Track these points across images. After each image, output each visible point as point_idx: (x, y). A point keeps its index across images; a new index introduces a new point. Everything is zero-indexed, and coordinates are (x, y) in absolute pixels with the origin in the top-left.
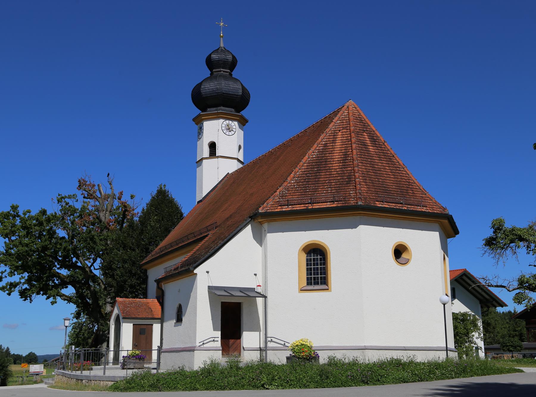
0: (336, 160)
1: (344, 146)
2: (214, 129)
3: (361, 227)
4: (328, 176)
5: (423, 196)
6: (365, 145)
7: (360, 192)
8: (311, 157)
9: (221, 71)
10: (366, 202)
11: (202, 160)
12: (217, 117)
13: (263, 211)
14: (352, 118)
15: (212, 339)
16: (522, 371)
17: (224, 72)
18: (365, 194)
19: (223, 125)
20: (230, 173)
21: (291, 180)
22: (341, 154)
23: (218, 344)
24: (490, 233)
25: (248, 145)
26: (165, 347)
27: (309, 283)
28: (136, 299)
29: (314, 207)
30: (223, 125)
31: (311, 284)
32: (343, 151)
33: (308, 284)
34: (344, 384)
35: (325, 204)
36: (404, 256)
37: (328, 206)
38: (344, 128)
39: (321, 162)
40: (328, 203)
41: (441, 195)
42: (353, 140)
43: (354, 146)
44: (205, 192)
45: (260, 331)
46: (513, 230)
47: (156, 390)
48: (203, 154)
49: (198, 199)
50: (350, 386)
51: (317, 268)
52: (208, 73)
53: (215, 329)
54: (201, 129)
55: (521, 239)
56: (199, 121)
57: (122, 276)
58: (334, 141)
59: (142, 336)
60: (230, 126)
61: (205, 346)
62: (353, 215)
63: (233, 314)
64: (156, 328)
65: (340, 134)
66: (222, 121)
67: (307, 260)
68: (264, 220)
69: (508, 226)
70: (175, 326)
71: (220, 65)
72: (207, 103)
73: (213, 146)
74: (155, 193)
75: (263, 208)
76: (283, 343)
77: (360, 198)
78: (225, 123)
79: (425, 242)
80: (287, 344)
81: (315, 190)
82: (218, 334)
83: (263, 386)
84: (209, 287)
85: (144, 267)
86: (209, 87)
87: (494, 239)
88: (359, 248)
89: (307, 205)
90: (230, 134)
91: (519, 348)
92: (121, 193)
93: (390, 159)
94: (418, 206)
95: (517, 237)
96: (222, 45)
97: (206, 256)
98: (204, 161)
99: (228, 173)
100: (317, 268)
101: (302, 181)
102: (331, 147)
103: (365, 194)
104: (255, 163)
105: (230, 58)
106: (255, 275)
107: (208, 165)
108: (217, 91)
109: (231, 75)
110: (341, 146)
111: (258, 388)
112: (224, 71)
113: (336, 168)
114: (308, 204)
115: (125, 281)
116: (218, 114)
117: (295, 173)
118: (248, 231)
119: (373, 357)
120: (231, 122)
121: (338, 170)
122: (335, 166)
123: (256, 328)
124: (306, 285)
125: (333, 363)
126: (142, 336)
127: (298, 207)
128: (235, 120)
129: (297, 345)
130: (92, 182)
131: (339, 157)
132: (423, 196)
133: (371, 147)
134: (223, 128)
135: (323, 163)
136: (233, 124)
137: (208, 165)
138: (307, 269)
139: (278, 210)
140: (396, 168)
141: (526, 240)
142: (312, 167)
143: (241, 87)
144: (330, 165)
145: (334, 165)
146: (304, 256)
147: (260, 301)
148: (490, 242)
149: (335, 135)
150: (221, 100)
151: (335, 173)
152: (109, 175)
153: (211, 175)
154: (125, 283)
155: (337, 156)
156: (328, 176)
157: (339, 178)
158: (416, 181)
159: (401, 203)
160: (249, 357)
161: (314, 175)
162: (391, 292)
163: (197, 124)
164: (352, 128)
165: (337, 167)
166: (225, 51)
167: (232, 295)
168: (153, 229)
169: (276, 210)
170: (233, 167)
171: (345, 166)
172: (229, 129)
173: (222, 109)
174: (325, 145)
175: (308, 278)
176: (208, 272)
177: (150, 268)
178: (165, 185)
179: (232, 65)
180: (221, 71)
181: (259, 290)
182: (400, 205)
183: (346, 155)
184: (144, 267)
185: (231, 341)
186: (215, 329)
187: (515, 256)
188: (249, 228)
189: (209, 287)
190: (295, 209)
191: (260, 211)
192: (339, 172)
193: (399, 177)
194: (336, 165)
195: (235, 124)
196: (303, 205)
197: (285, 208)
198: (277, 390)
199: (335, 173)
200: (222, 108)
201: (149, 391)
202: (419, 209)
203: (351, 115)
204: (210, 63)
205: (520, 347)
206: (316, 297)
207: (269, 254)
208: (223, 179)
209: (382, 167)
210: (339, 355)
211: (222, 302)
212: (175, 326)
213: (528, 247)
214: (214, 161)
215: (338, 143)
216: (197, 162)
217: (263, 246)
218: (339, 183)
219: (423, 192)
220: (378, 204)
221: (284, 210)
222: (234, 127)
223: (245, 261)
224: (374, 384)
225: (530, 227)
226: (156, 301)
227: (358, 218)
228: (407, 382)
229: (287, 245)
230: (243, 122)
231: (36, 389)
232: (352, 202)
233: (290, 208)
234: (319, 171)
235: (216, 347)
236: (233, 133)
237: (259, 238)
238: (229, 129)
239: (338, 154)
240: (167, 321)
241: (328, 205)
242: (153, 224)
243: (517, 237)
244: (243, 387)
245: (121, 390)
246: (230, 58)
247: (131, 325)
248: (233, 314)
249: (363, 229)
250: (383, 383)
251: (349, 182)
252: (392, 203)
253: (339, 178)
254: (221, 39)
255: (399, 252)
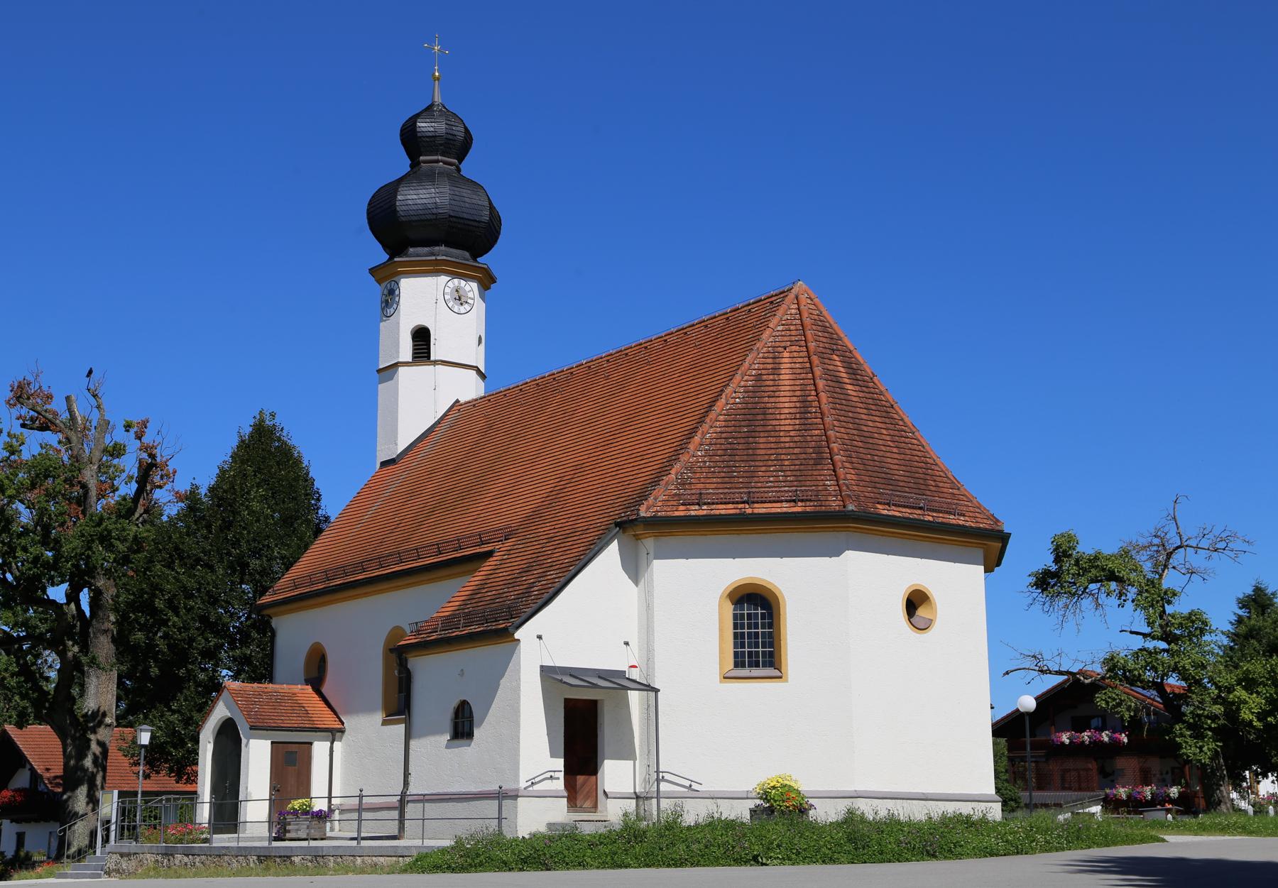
0: (786, 411)
1: (798, 382)
2: (425, 297)
3: (849, 554)
4: (772, 445)
5: (955, 491)
6: (838, 381)
7: (842, 485)
8: (732, 401)
9: (437, 161)
10: (859, 505)
11: (396, 365)
12: (434, 269)
13: (648, 515)
14: (807, 321)
15: (548, 775)
16: (1164, 840)
17: (445, 163)
18: (855, 488)
19: (447, 290)
20: (462, 401)
21: (696, 450)
22: (795, 399)
23: (559, 785)
24: (1047, 561)
25: (493, 338)
26: (413, 790)
27: (739, 663)
28: (266, 685)
29: (756, 511)
30: (447, 290)
31: (743, 666)
32: (798, 393)
33: (736, 665)
34: (898, 858)
35: (779, 505)
36: (921, 612)
37: (785, 510)
38: (793, 343)
39: (754, 415)
40: (785, 504)
41: (988, 491)
42: (818, 371)
43: (821, 384)
44: (404, 440)
45: (634, 759)
46: (1096, 558)
47: (537, 869)
48: (398, 352)
49: (383, 456)
50: (907, 860)
51: (756, 632)
52: (404, 165)
53: (553, 755)
54: (390, 299)
55: (1112, 576)
56: (386, 277)
57: (186, 628)
58: (776, 371)
59: (291, 769)
60: (461, 292)
61: (536, 787)
62: (834, 529)
63: (583, 728)
64: (320, 749)
65: (786, 354)
66: (444, 279)
67: (735, 616)
68: (644, 529)
69: (1085, 548)
70: (447, 747)
71: (432, 145)
72: (403, 237)
73: (422, 337)
74: (247, 430)
75: (648, 508)
76: (687, 783)
77: (849, 496)
78: (450, 284)
79: (958, 584)
80: (695, 786)
81: (752, 475)
82: (559, 763)
83: (755, 858)
84: (542, 667)
85: (266, 612)
86: (414, 198)
87: (1056, 575)
88: (838, 593)
89: (740, 506)
90: (462, 309)
91: (1013, 803)
92: (144, 424)
93: (886, 411)
94: (950, 513)
95: (1105, 573)
96: (438, 99)
97: (540, 602)
98: (402, 371)
99: (457, 401)
100: (756, 632)
101: (719, 452)
102: (771, 383)
103: (855, 488)
104: (546, 387)
105: (459, 132)
106: (627, 644)
107: (411, 379)
108: (435, 211)
109: (459, 170)
110: (792, 382)
111: (746, 862)
112: (440, 162)
113: (787, 428)
114: (743, 502)
115: (191, 640)
116: (437, 262)
117: (704, 434)
118: (611, 555)
119: (917, 812)
120: (463, 283)
121: (792, 433)
122: (786, 424)
123: (627, 753)
124: (732, 666)
125: (851, 821)
126: (291, 769)
127: (722, 510)
128: (472, 278)
129: (774, 787)
130: (45, 388)
131: (792, 405)
132: (955, 491)
133: (849, 387)
134: (447, 297)
135: (759, 417)
136: (467, 288)
137: (411, 379)
138: (736, 635)
139: (682, 514)
140: (900, 433)
141: (1119, 580)
142: (737, 423)
143: (487, 204)
144: (774, 423)
145: (783, 422)
146: (729, 608)
147: (634, 697)
148: (1044, 581)
149: (776, 358)
150: (432, 228)
151: (788, 439)
152: (90, 372)
153: (419, 403)
154: (190, 646)
155: (786, 403)
156: (772, 445)
157: (796, 451)
158: (938, 461)
159: (920, 508)
160: (614, 812)
161: (742, 441)
162: (896, 684)
163: (379, 282)
164: (812, 345)
165: (791, 428)
166: (448, 115)
167: (595, 686)
168: (258, 521)
169: (677, 514)
170: (469, 388)
171: (805, 427)
172: (459, 299)
173: (443, 252)
174: (758, 378)
175: (736, 654)
176: (540, 637)
177: (277, 615)
178: (273, 415)
179: (459, 147)
180: (437, 161)
181: (635, 674)
182: (919, 512)
183: (804, 404)
184: (266, 612)
185: (580, 779)
186: (553, 755)
187: (1098, 613)
188: (614, 547)
189: (542, 667)
190: (717, 512)
191: (642, 514)
192: (796, 439)
193: (908, 452)
194: (787, 422)
195: (471, 288)
196: (731, 506)
197: (694, 511)
198: (782, 867)
199: (788, 439)
200: (443, 248)
201: (521, 870)
202: (952, 519)
203: (805, 315)
204: (411, 140)
205: (1015, 800)
206: (756, 692)
207: (657, 603)
208: (445, 415)
209: (875, 430)
210: (867, 808)
211: (567, 701)
212: (447, 747)
213: (1121, 594)
214: (423, 370)
215: (785, 376)
216: (379, 371)
217: (642, 584)
218: (797, 462)
219: (955, 485)
220: (883, 511)
221: (693, 513)
222: (470, 295)
223: (598, 616)
224: (945, 858)
225: (1127, 553)
226: (309, 689)
227: (842, 536)
228: (997, 855)
229: (695, 586)
230: (486, 281)
231: (36, 885)
232: (834, 504)
233: (704, 511)
234: (752, 433)
235: (557, 791)
236: (467, 307)
237: (634, 569)
238: (459, 299)
239: (787, 399)
240: (420, 736)
241: (784, 508)
242: (256, 506)
243: (1105, 573)
244: (716, 862)
245: (453, 871)
246: (460, 135)
247: (267, 745)
248: (583, 728)
249: (853, 558)
250: (959, 856)
251: (818, 462)
252: (905, 507)
253: (796, 451)
254: (437, 82)
255: (915, 603)
